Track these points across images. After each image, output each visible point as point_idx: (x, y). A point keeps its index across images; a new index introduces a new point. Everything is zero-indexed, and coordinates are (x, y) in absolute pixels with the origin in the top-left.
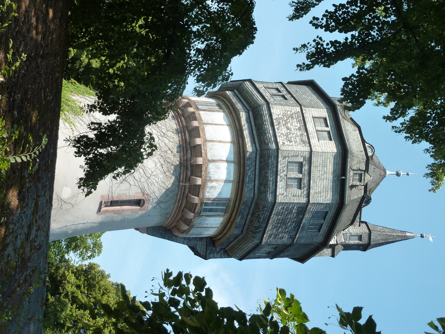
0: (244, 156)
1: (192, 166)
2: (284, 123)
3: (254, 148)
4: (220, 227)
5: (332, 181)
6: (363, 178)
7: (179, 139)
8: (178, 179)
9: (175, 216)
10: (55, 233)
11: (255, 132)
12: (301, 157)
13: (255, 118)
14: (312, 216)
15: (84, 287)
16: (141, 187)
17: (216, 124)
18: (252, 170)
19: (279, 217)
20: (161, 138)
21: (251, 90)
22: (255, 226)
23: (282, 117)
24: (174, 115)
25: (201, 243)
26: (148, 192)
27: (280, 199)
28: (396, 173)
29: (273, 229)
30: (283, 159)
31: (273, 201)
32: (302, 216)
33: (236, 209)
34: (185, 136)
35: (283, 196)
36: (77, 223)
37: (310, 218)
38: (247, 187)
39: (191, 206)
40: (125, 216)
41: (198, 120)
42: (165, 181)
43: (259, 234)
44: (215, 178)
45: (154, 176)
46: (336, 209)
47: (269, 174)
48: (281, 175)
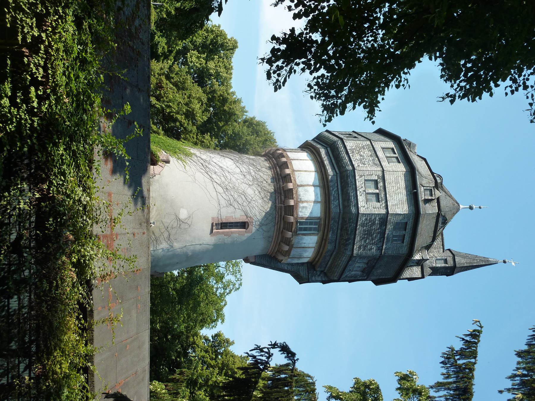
0: (327, 178)
1: (285, 191)
3: (335, 172)
4: (316, 248)
6: (433, 193)
8: (274, 207)
11: (333, 161)
15: (212, 353)
19: (365, 228)
25: (302, 268)
26: (251, 215)
27: (362, 210)
29: (361, 240)
33: (326, 227)
35: (364, 208)
36: (194, 244)
44: (305, 200)
45: (254, 201)
46: (413, 219)
48: (360, 190)
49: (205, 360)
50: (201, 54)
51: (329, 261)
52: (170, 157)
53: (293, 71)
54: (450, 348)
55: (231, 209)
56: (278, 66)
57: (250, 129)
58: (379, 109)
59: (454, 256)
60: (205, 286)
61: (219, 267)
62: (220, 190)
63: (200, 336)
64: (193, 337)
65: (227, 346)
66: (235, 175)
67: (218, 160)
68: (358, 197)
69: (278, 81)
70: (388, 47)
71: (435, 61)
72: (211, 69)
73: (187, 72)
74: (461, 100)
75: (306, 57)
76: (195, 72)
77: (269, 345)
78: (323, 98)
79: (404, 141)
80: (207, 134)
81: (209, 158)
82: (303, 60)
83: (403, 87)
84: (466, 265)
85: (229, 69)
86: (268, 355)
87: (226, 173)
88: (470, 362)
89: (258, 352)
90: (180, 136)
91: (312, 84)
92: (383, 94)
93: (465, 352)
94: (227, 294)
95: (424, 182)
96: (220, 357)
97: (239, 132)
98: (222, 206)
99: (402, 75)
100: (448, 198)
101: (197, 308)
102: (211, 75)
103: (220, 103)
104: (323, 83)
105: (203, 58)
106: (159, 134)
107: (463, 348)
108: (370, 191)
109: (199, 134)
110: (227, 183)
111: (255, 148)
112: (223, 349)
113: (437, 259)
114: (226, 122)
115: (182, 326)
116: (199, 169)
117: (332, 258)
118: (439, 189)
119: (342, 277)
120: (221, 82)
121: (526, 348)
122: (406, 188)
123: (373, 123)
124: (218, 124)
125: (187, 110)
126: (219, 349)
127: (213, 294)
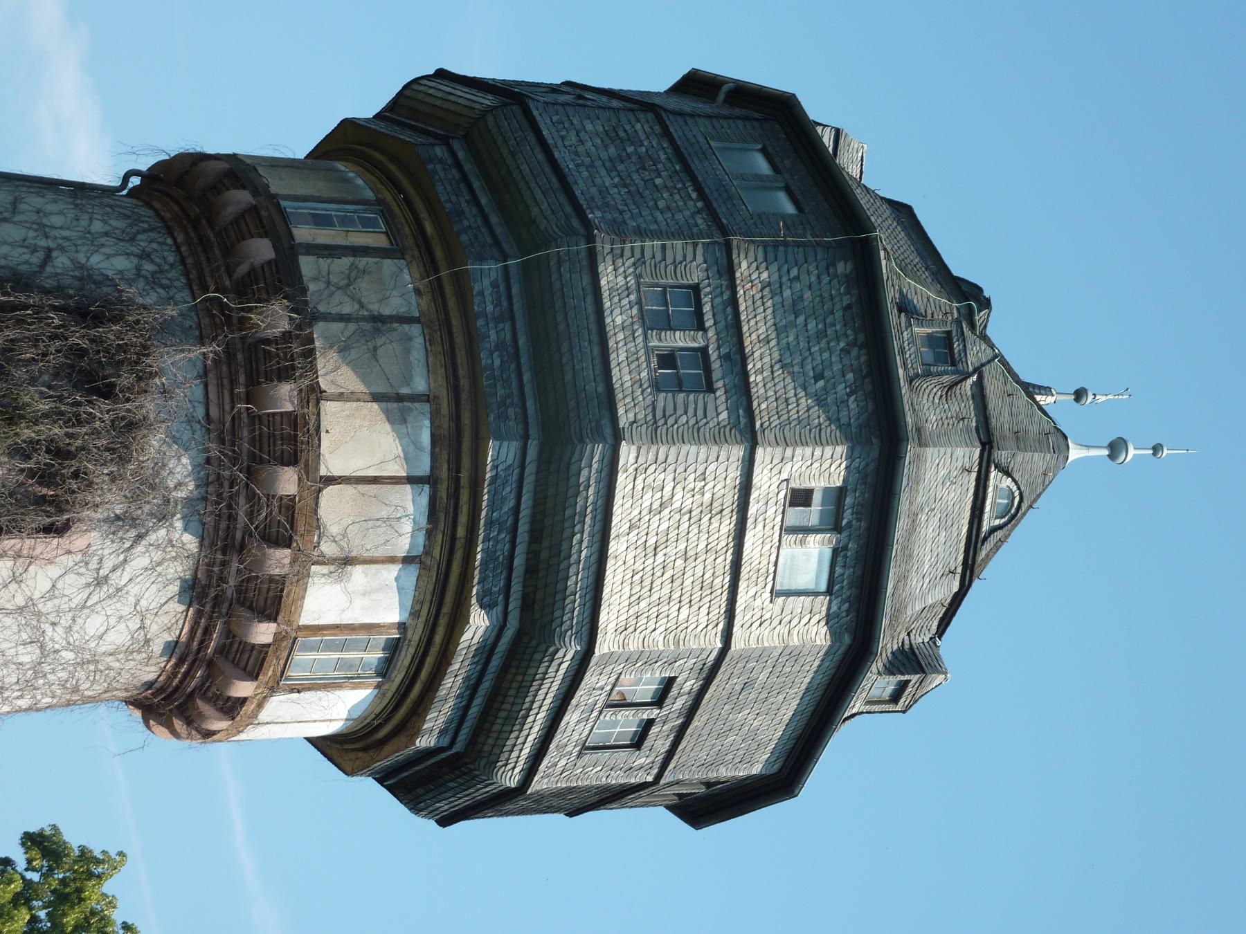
24: (184, 638)
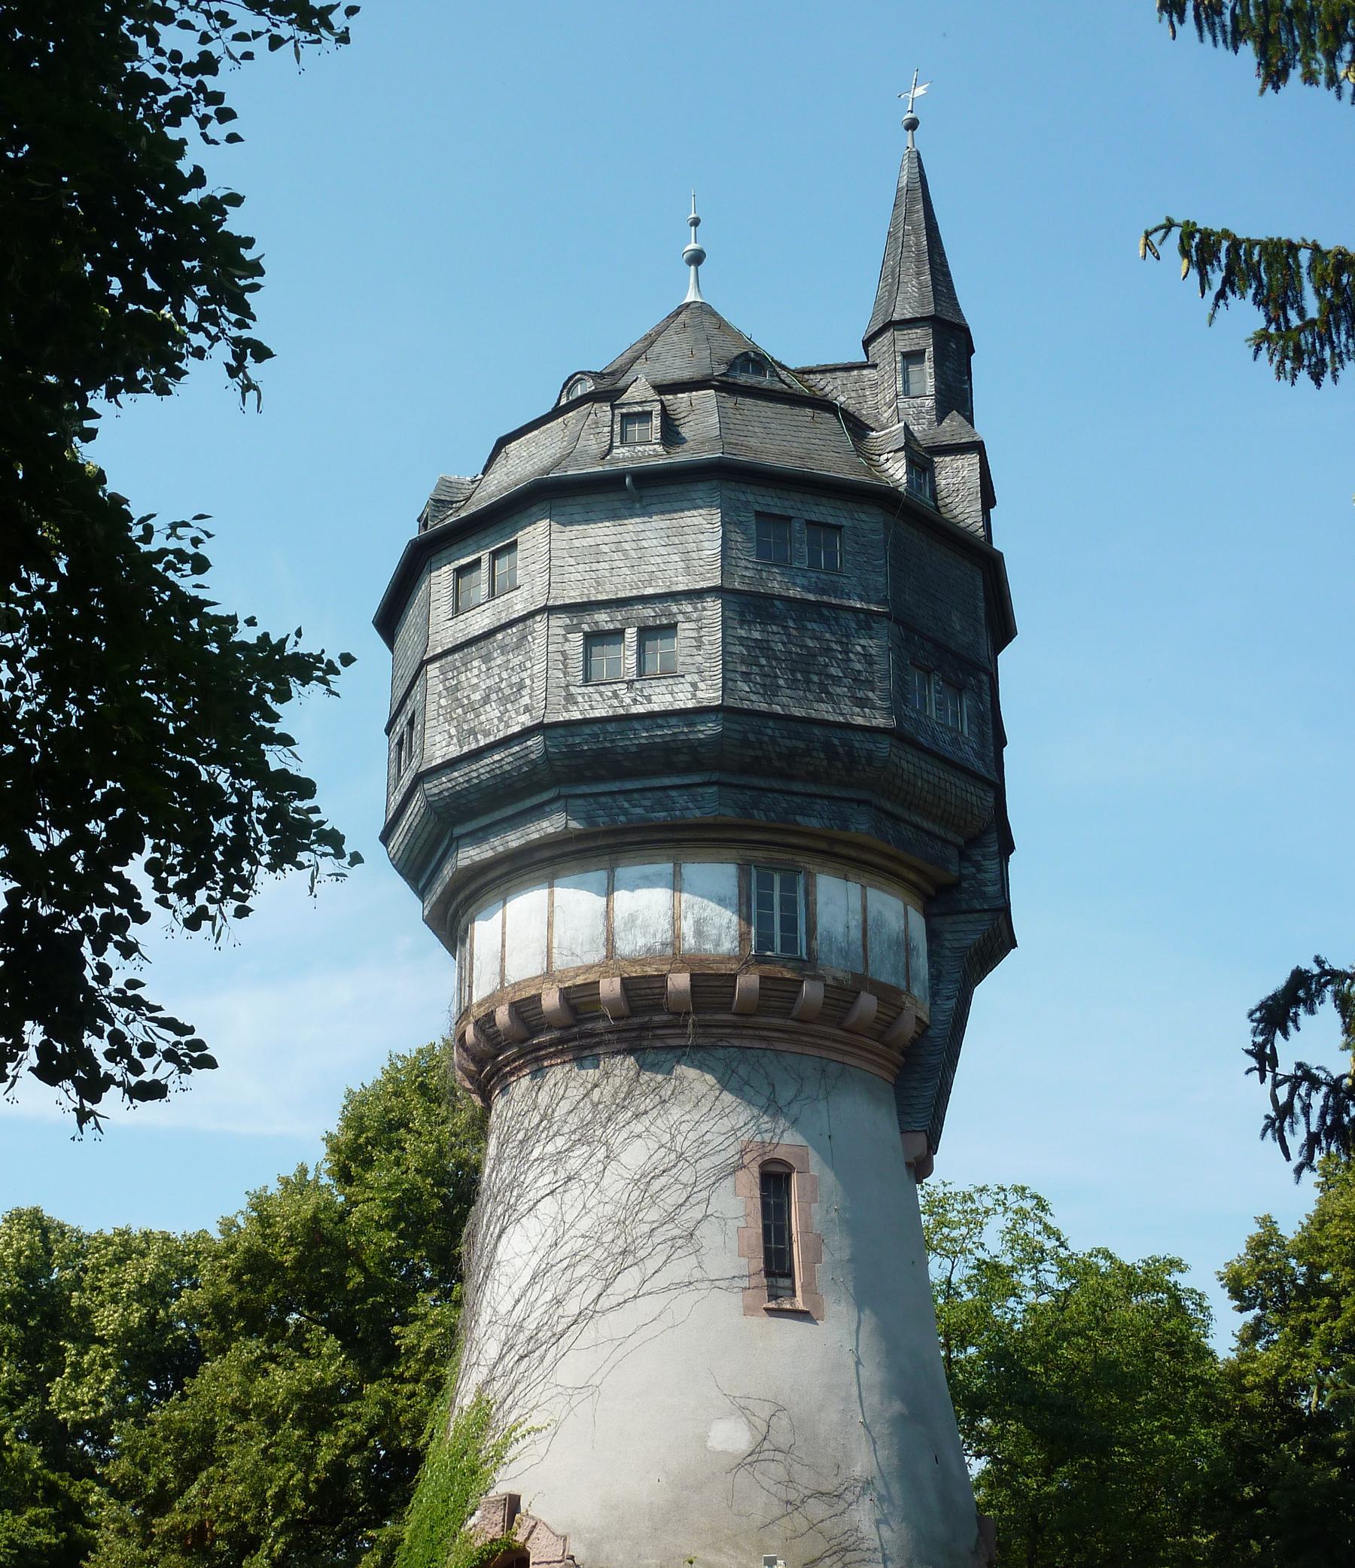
0: (580, 837)
1: (634, 1012)
2: (472, 716)
3: (554, 806)
4: (864, 881)
5: (646, 519)
7: (557, 1064)
8: (698, 1054)
9: (827, 1043)
10: (896, 1461)
12: (567, 640)
13: (470, 814)
14: (777, 566)
15: (1312, 1309)
16: (714, 1178)
17: (503, 946)
18: (626, 805)
19: (781, 682)
20: (555, 1127)
21: (402, 836)
22: (825, 763)
23: (455, 723)
25: (948, 936)
26: (732, 1151)
27: (710, 694)
28: (693, 267)
29: (831, 698)
30: (576, 703)
31: (720, 716)
32: (777, 603)
33: (778, 838)
34: (545, 1047)
35: (702, 685)
36: (855, 1389)
37: (782, 574)
38: (687, 813)
39: (786, 994)
40: (832, 1220)
41: (493, 1008)
42: (693, 1098)
43: (857, 745)
44: (667, 926)
45: (673, 1138)
47: (628, 743)
48: (628, 701)
49: (1339, 1338)
50: (63, 1365)
51: (917, 827)
52: (492, 1494)
53: (130, 993)
54: (1258, 349)
55: (708, 1233)
56: (110, 1056)
57: (376, 1154)
58: (293, 638)
59: (889, 325)
60: (1030, 1342)
61: (949, 1281)
62: (628, 1281)
63: (1243, 1360)
64: (1244, 1389)
65: (1282, 1246)
66: (569, 1219)
67: (502, 1290)
68: (657, 709)
69: (170, 1056)
70: (39, 605)
71: (99, 416)
72: (124, 1322)
73: (139, 1425)
74: (254, 319)
75: (76, 939)
76: (139, 1388)
77: (1262, 1080)
78: (246, 865)
79: (425, 525)
80: (397, 1337)
81: (497, 1328)
82: (87, 950)
83: (201, 541)
84: (927, 277)
85: (125, 1244)
86: (1305, 1085)
87: (560, 1256)
88: (1312, 268)
89: (1291, 1125)
90: (406, 1450)
91: (186, 910)
92: (232, 620)
93: (1270, 290)
94: (1062, 1245)
95: (593, 444)
96: (1326, 1277)
97: (387, 1203)
98: (697, 1274)
99: (154, 547)
100: (657, 348)
101: (1125, 1375)
102: (151, 1320)
103: (266, 1285)
104: (185, 866)
105: (81, 1354)
106: (396, 1542)
107: (1255, 295)
108: (631, 661)
109: (397, 1371)
110: (599, 1254)
111: (456, 1135)
112: (1293, 1262)
113: (906, 392)
114: (350, 1255)
115: (1202, 1435)
116: (540, 1370)
117: (906, 815)
118: (621, 384)
119: (983, 771)
120: (179, 1281)
121: (1248, 50)
122: (620, 518)
123: (347, 659)
124: (355, 1291)
125: (297, 1422)
126: (1293, 1282)
127: (1062, 1309)
